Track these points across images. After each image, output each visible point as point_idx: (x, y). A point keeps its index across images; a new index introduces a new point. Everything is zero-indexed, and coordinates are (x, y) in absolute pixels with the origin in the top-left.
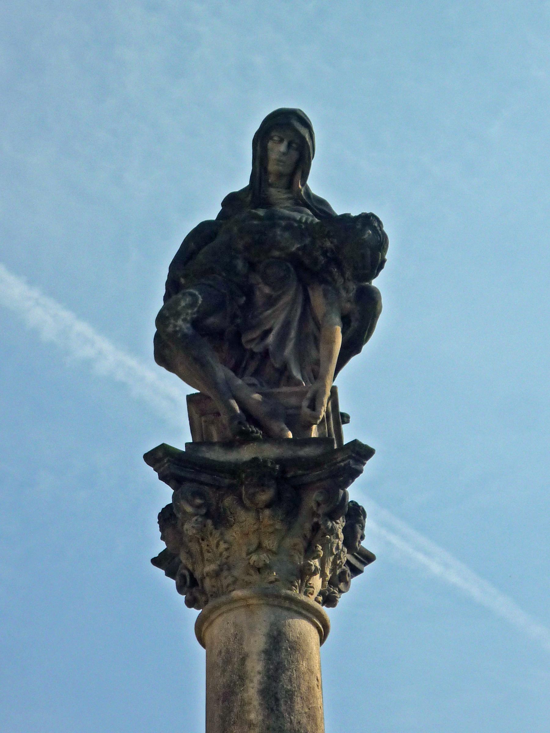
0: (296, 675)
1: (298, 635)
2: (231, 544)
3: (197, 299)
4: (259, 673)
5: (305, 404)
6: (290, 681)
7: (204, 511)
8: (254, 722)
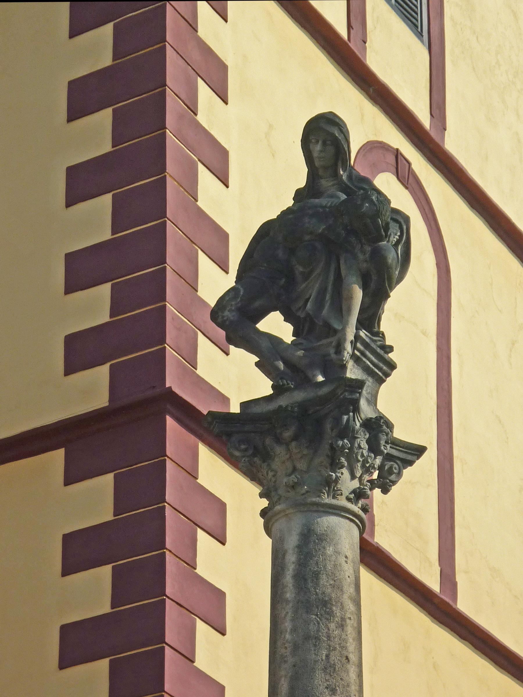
0: (322, 559)
1: (326, 529)
2: (276, 472)
3: (239, 291)
4: (293, 563)
5: (332, 351)
6: (317, 563)
7: (250, 452)
8: (289, 599)
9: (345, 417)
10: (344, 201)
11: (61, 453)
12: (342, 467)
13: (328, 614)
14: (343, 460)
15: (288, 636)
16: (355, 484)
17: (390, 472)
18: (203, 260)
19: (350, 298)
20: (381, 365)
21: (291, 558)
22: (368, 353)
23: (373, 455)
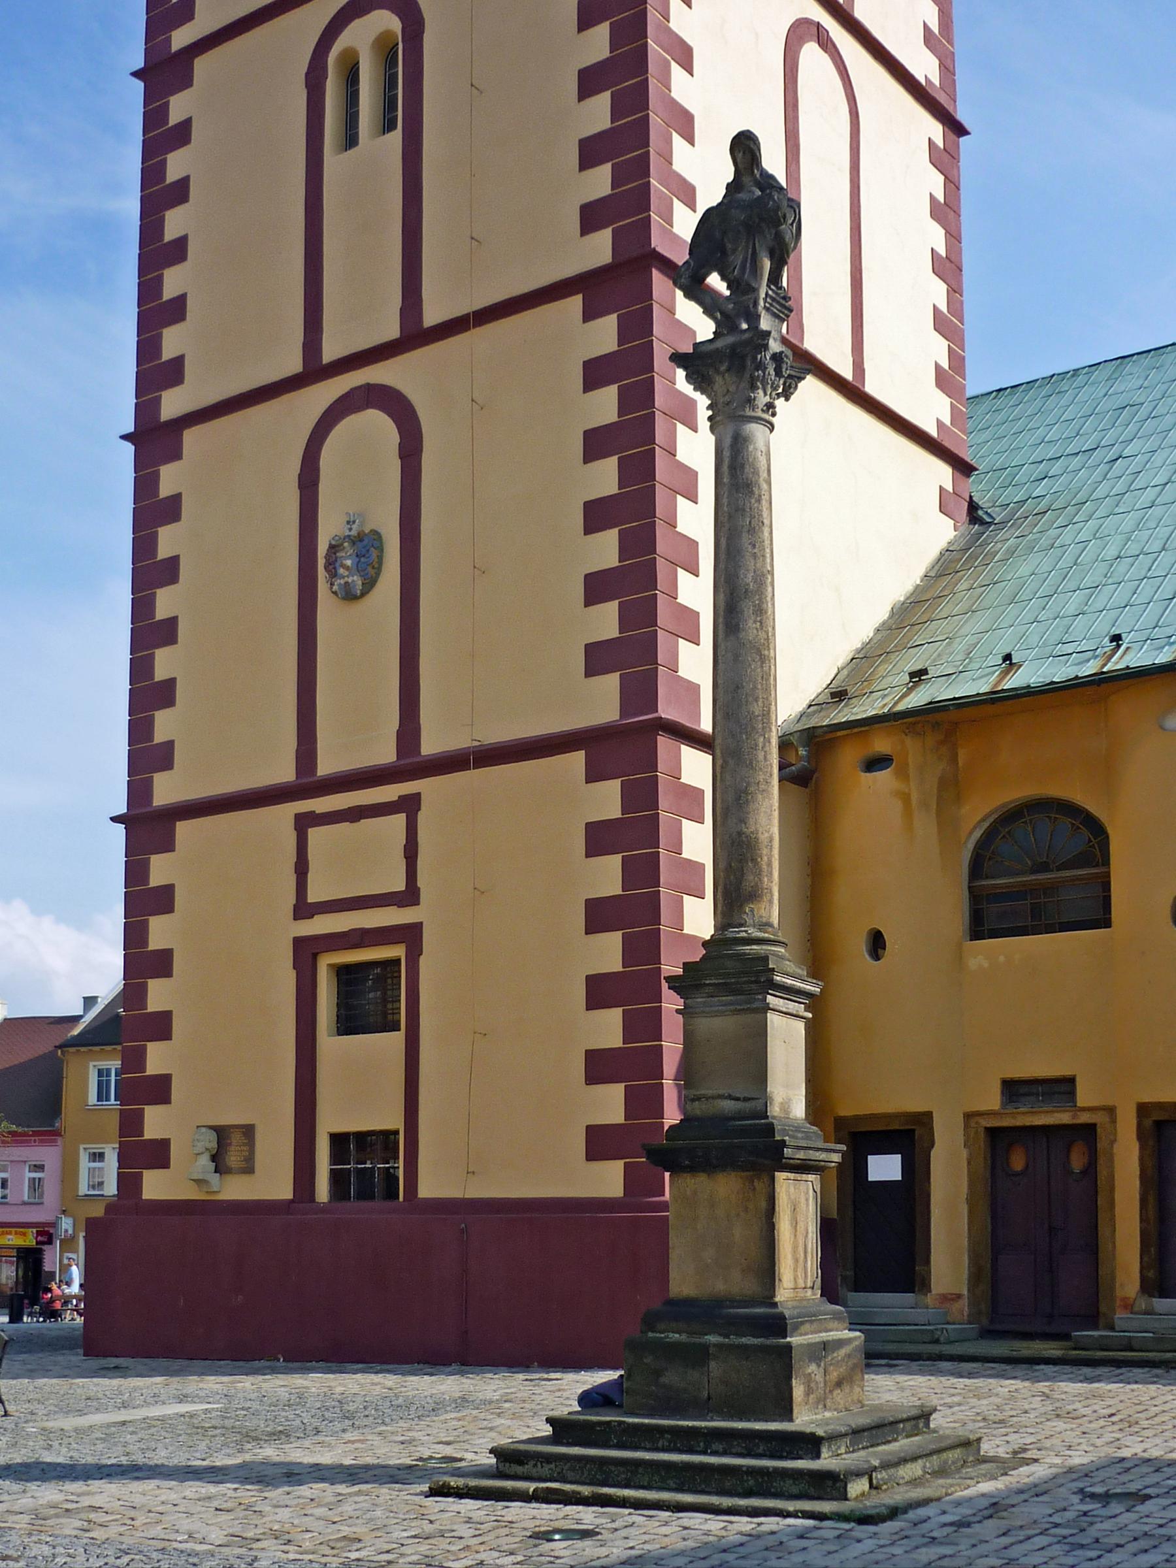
5: (751, 306)
6: (743, 457)
9: (759, 356)
10: (759, 197)
11: (579, 297)
12: (758, 388)
13: (750, 492)
14: (759, 384)
15: (726, 509)
16: (767, 399)
17: (790, 387)
18: (676, 138)
19: (762, 268)
20: (783, 310)
21: (727, 454)
22: (774, 304)
23: (778, 379)
